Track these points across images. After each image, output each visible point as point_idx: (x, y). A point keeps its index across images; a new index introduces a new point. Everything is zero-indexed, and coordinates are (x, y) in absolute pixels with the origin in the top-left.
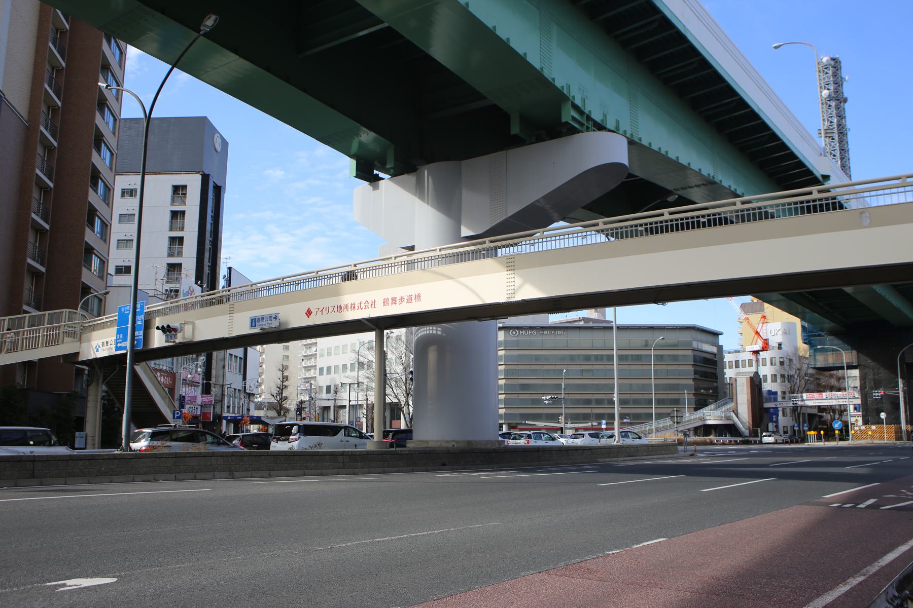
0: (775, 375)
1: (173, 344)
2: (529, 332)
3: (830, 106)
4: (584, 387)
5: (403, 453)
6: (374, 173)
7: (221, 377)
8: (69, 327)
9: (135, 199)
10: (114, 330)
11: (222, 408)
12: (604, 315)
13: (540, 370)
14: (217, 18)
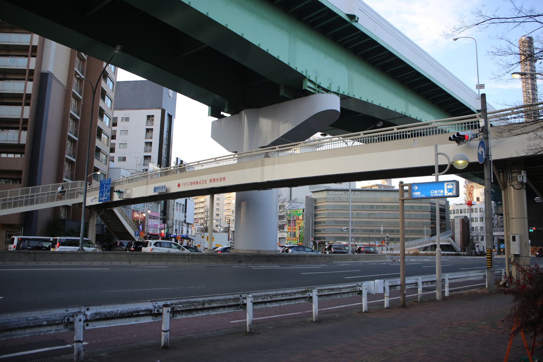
0: (482, 218)
1: (122, 199)
2: (340, 192)
3: (526, 64)
4: (371, 223)
5: (220, 255)
6: (221, 114)
7: (172, 215)
8: (81, 189)
9: (128, 123)
10: (98, 191)
11: (172, 230)
12: (391, 183)
13: (346, 213)
14: (121, 47)
